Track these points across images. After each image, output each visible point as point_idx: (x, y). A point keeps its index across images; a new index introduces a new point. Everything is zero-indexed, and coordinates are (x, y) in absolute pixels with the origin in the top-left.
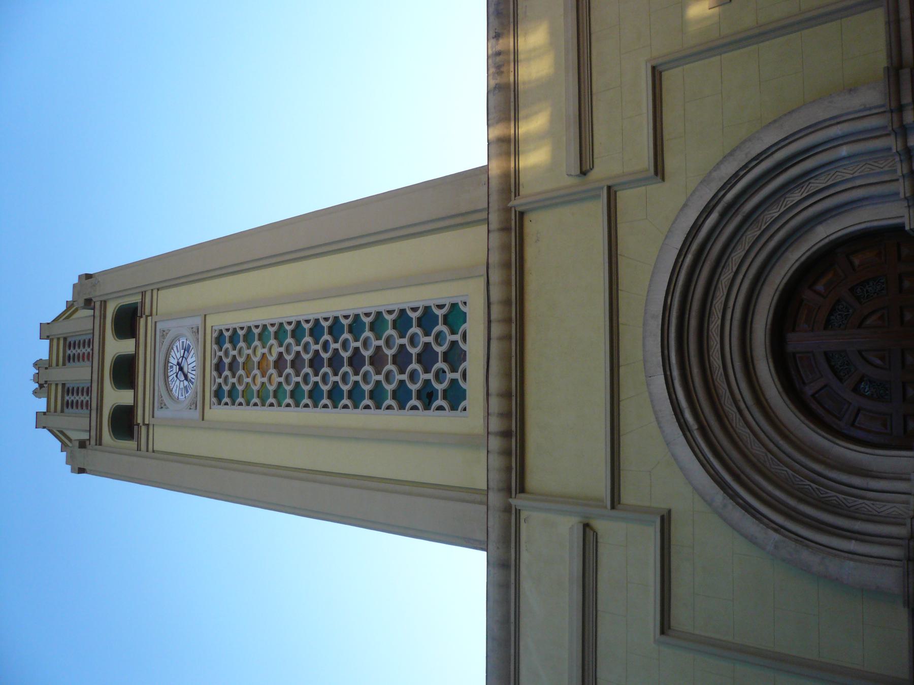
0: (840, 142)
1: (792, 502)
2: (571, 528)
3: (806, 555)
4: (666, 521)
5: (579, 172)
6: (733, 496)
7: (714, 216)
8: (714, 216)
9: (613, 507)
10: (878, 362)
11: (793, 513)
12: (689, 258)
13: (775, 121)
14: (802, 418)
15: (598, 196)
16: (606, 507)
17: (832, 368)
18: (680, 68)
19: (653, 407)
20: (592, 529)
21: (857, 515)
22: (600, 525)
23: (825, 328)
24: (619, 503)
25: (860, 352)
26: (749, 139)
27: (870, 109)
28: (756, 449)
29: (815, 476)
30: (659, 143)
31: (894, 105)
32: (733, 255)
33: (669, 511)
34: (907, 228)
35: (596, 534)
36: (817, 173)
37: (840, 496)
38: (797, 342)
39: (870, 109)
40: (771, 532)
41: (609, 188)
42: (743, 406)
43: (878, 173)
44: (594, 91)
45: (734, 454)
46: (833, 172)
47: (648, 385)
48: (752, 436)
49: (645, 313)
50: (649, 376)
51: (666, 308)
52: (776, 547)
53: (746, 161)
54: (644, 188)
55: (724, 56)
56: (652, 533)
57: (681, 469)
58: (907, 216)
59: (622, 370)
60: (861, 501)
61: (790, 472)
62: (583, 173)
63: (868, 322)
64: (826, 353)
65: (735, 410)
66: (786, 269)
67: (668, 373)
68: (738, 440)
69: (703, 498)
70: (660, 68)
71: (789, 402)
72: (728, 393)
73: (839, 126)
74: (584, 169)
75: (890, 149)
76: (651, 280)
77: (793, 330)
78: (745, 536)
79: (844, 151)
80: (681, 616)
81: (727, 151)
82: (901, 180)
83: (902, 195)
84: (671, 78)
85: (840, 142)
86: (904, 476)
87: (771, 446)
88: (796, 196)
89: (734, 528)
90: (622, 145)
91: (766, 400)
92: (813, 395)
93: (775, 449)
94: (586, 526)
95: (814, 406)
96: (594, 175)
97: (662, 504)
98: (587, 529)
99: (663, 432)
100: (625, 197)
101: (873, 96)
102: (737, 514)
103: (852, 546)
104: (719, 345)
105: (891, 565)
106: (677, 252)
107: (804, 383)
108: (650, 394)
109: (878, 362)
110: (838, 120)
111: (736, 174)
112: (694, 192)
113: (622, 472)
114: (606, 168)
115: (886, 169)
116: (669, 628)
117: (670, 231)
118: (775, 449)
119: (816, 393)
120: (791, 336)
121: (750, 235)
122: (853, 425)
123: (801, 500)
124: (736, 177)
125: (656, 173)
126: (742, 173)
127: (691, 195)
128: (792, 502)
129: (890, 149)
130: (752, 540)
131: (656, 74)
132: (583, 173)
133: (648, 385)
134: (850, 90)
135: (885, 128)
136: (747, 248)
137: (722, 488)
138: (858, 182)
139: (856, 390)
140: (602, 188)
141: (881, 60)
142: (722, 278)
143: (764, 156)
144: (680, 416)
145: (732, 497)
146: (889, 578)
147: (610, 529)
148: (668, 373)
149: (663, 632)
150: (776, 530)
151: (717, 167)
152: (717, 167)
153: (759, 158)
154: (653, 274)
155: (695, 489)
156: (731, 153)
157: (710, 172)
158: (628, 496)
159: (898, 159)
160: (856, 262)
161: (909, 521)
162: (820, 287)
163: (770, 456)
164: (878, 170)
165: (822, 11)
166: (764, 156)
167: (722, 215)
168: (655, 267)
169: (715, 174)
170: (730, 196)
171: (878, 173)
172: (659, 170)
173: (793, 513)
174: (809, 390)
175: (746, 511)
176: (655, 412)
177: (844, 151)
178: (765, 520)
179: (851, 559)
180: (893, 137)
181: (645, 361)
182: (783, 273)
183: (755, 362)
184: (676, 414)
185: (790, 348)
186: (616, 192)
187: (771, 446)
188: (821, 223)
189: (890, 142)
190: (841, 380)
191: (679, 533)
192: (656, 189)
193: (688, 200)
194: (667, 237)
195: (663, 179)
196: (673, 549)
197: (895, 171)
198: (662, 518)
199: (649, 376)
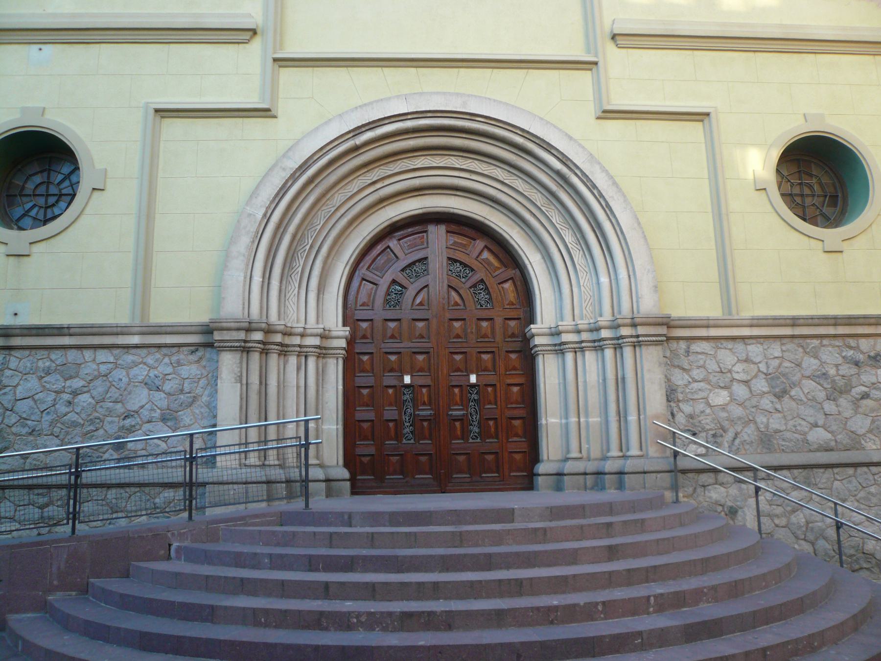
0: (613, 277)
1: (292, 229)
2: (250, 16)
3: (245, 241)
4: (265, 113)
5: (616, 32)
6: (294, 177)
7: (558, 165)
8: (558, 165)
9: (275, 60)
10: (418, 301)
11: (282, 230)
12: (519, 140)
13: (639, 224)
14: (368, 238)
15: (588, 51)
16: (275, 53)
17: (414, 263)
18: (703, 140)
19: (377, 101)
20: (252, 38)
21: (284, 282)
22: (256, 44)
23: (449, 259)
24: (280, 67)
25: (427, 286)
26: (626, 200)
27: (637, 302)
28: (338, 198)
29: (316, 248)
30: (634, 116)
31: (637, 320)
32: (520, 180)
33: (275, 117)
34: (532, 326)
35: (247, 42)
36: (588, 256)
37: (300, 269)
38: (437, 234)
39: (637, 302)
40: (263, 210)
41: (596, 63)
42: (378, 186)
43: (581, 306)
44: (696, 52)
45: (333, 178)
46: (587, 269)
47: (398, 97)
48: (350, 194)
49: (469, 96)
50: (406, 97)
51: (472, 116)
52: (250, 215)
53: (606, 197)
54: (592, 99)
55: (707, 181)
56: (253, 101)
57: (317, 129)
58: (542, 326)
59: (413, 70)
60: (297, 285)
61: (319, 227)
62: (614, 37)
63: (453, 293)
64: (426, 258)
65: (375, 179)
66: (504, 228)
67: (409, 117)
68: (345, 236)
69: (289, 149)
70: (706, 121)
71: (382, 226)
72: (390, 173)
73: (626, 277)
74: (617, 38)
75: (601, 316)
76: (501, 102)
77: (448, 232)
78: (257, 187)
79: (604, 280)
80: (174, 128)
81: (617, 180)
82: (573, 323)
83: (560, 323)
84: (695, 130)
85: (613, 277)
86: (320, 319)
87: (342, 211)
88: (569, 238)
89: (264, 177)
90: (636, 78)
91: (384, 207)
92: (389, 247)
93: (339, 214)
94: (254, 32)
95: (379, 248)
96: (610, 47)
97: (282, 108)
98: (251, 33)
99: (352, 110)
100: (585, 77)
101: (648, 305)
102: (277, 180)
103: (257, 279)
104: (435, 165)
105: (244, 308)
106: (527, 128)
107: (399, 240)
108: (388, 99)
109: (418, 301)
110: (632, 277)
111: (595, 187)
112: (583, 147)
113: (310, 69)
114: (616, 60)
115: (584, 312)
116: (162, 117)
117: (548, 123)
118: (339, 214)
119: (392, 251)
120: (442, 228)
121: (538, 198)
122: (363, 279)
123: (294, 236)
124: (592, 187)
125: (605, 112)
126: (595, 192)
127: (580, 145)
128: (292, 229)
129: (601, 316)
130: (254, 193)
131: (702, 116)
132: (614, 37)
133: (398, 97)
134: (656, 287)
135: (620, 313)
136: (526, 193)
137: (300, 167)
138: (575, 290)
139: (394, 282)
140: (596, 56)
141: (677, 312)
142: (499, 170)
143: (608, 212)
144: (367, 128)
145: (293, 175)
146: (233, 308)
147: (251, 57)
148: (409, 117)
149: (157, 111)
150: (265, 215)
151: (604, 170)
152: (604, 170)
153: (607, 208)
154: (506, 104)
155: (298, 142)
156: (615, 183)
157: (599, 163)
158: (287, 75)
159: (592, 321)
160: (507, 285)
161: (283, 323)
162: (486, 255)
163: (333, 209)
164: (584, 305)
165: (730, 267)
166: (608, 212)
167: (558, 173)
168: (513, 106)
169: (597, 167)
170: (575, 180)
171: (581, 306)
172: (608, 114)
173: (282, 230)
174: (393, 243)
175: (281, 189)
176: (371, 103)
177: (604, 280)
178: (273, 206)
179: (245, 278)
180: (611, 318)
181: (421, 94)
182: (500, 224)
183: (419, 198)
184: (369, 123)
185: (431, 228)
186: (591, 70)
187: (342, 211)
188: (543, 258)
189: (607, 316)
190: (403, 270)
191: (254, 126)
192: (591, 110)
193: (575, 141)
194: (542, 119)
195: (598, 118)
196: (239, 121)
197: (582, 319)
198: (268, 110)
199: (406, 97)
